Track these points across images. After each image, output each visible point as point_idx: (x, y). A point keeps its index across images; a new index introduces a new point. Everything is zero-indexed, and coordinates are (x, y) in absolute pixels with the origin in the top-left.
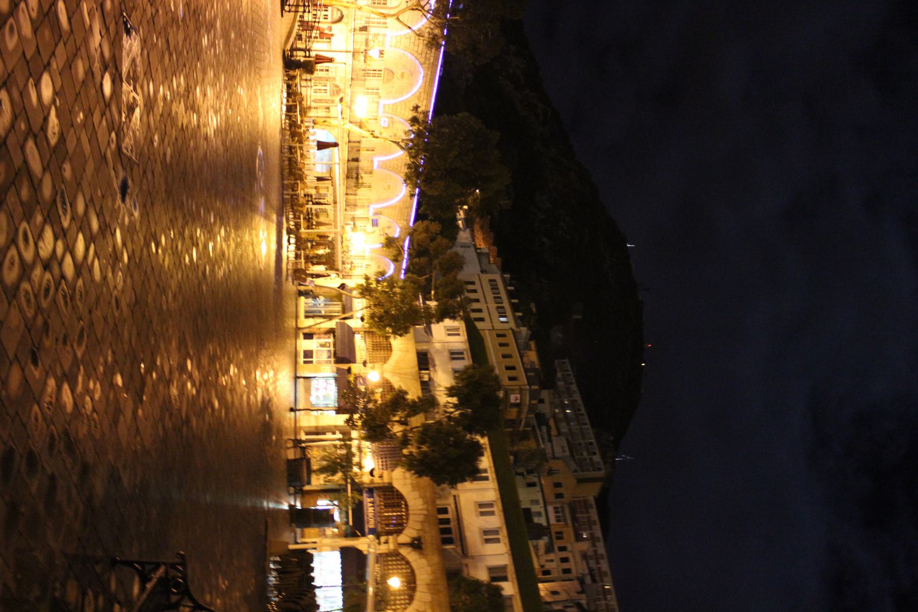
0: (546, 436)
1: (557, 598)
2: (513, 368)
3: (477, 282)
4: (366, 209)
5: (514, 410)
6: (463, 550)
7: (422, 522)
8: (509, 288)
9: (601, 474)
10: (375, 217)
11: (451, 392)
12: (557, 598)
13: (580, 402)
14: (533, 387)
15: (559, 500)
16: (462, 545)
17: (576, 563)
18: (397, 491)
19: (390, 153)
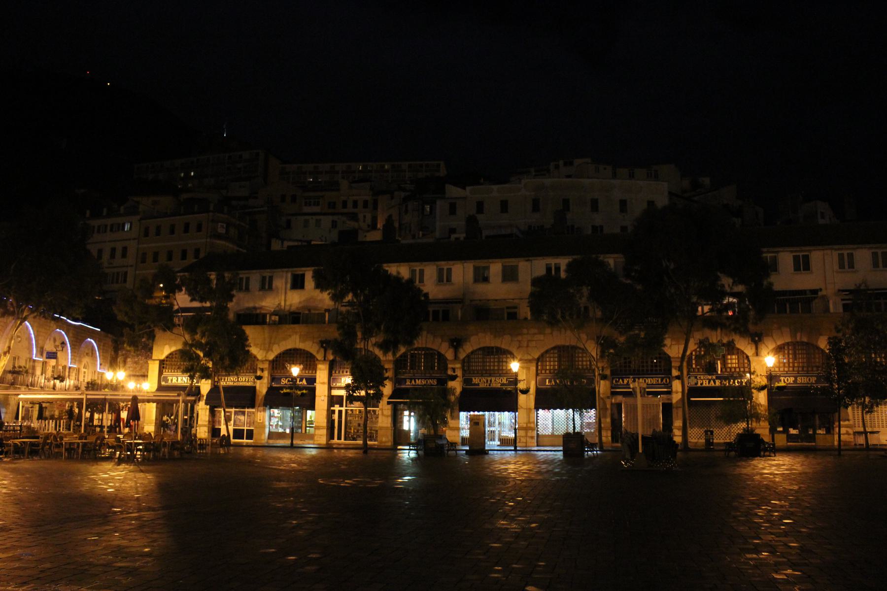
4: (36, 364)
6: (456, 303)
10: (45, 355)
16: (451, 303)
18: (277, 357)
19: (27, 327)
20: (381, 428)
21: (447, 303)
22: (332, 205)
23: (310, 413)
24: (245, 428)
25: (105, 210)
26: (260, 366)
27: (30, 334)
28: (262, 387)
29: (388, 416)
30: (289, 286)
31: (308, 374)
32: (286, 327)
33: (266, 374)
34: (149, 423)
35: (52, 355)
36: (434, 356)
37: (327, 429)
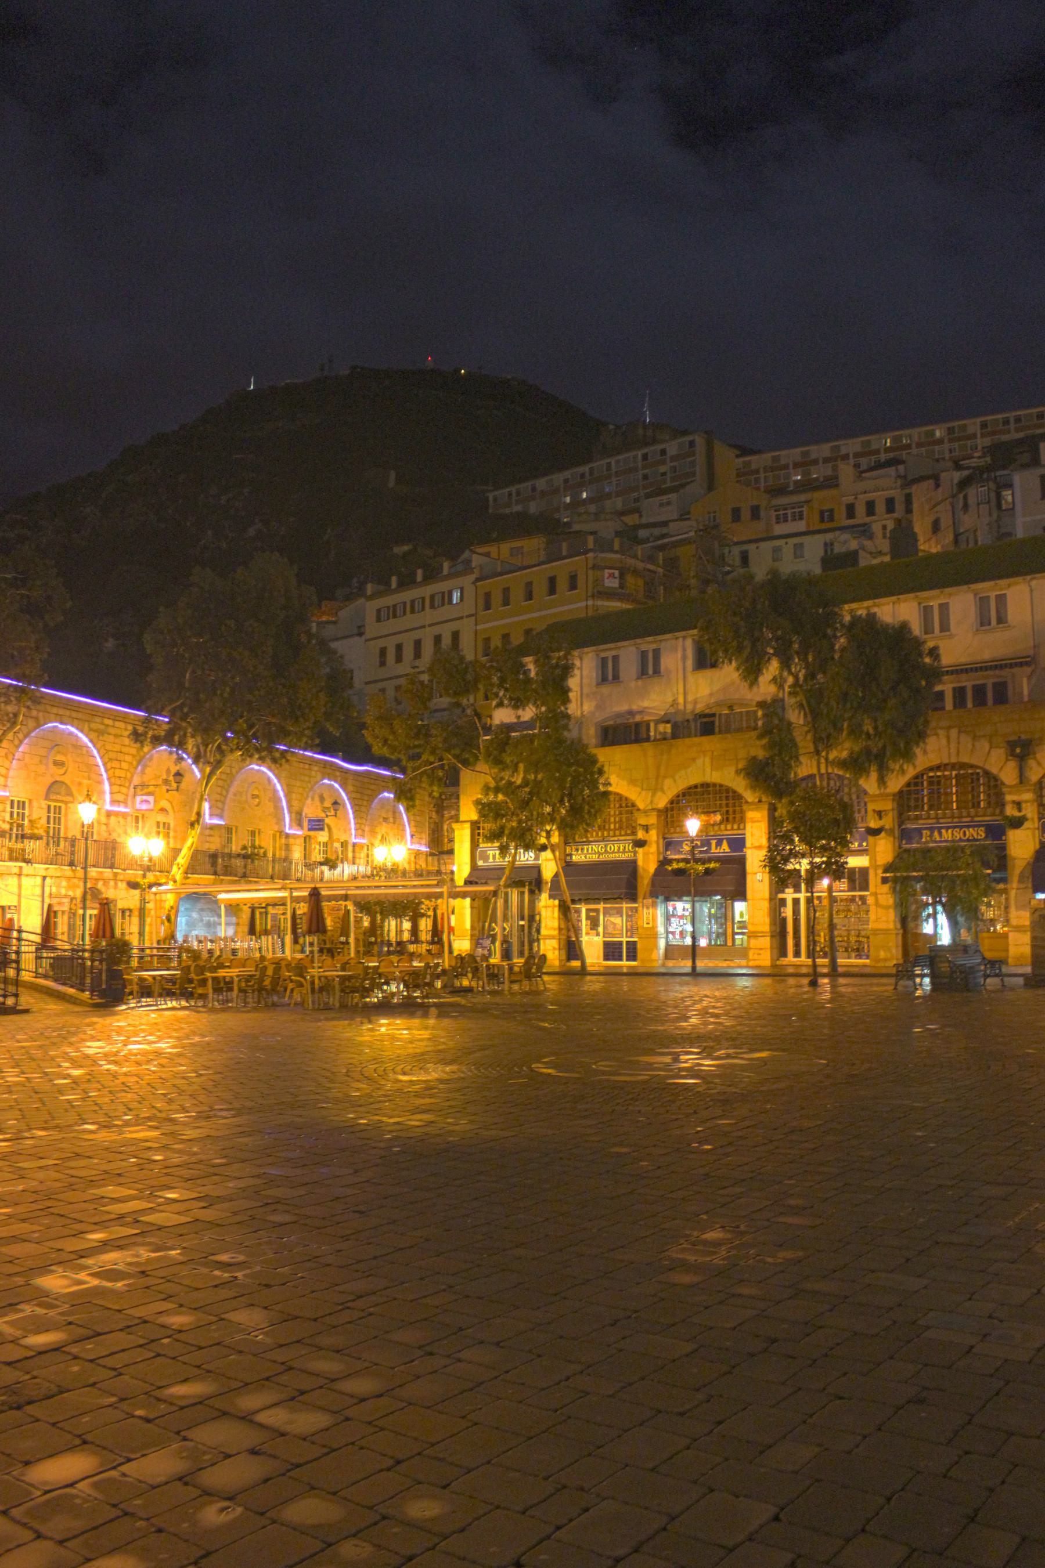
0: (657, 531)
1: (946, 521)
2: (552, 581)
3: (381, 643)
5: (630, 580)
6: (1021, 664)
7: (975, 738)
8: (394, 585)
9: (699, 440)
10: (305, 824)
11: (752, 672)
12: (946, 521)
13: (567, 474)
14: (591, 545)
15: (762, 513)
16: (1011, 666)
17: (877, 490)
20: (876, 932)
21: (1001, 667)
22: (826, 516)
23: (740, 907)
24: (624, 940)
25: (420, 573)
26: (642, 821)
27: (275, 791)
28: (648, 861)
29: (887, 908)
30: (690, 663)
31: (730, 830)
32: (682, 744)
33: (653, 835)
34: (461, 937)
35: (317, 825)
36: (979, 783)
37: (772, 936)
